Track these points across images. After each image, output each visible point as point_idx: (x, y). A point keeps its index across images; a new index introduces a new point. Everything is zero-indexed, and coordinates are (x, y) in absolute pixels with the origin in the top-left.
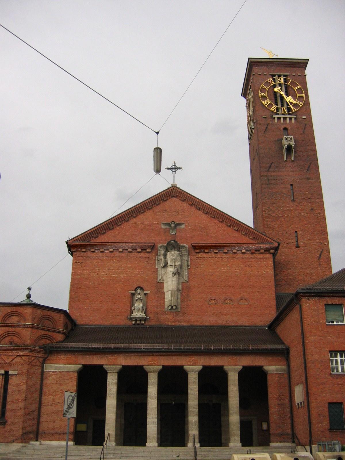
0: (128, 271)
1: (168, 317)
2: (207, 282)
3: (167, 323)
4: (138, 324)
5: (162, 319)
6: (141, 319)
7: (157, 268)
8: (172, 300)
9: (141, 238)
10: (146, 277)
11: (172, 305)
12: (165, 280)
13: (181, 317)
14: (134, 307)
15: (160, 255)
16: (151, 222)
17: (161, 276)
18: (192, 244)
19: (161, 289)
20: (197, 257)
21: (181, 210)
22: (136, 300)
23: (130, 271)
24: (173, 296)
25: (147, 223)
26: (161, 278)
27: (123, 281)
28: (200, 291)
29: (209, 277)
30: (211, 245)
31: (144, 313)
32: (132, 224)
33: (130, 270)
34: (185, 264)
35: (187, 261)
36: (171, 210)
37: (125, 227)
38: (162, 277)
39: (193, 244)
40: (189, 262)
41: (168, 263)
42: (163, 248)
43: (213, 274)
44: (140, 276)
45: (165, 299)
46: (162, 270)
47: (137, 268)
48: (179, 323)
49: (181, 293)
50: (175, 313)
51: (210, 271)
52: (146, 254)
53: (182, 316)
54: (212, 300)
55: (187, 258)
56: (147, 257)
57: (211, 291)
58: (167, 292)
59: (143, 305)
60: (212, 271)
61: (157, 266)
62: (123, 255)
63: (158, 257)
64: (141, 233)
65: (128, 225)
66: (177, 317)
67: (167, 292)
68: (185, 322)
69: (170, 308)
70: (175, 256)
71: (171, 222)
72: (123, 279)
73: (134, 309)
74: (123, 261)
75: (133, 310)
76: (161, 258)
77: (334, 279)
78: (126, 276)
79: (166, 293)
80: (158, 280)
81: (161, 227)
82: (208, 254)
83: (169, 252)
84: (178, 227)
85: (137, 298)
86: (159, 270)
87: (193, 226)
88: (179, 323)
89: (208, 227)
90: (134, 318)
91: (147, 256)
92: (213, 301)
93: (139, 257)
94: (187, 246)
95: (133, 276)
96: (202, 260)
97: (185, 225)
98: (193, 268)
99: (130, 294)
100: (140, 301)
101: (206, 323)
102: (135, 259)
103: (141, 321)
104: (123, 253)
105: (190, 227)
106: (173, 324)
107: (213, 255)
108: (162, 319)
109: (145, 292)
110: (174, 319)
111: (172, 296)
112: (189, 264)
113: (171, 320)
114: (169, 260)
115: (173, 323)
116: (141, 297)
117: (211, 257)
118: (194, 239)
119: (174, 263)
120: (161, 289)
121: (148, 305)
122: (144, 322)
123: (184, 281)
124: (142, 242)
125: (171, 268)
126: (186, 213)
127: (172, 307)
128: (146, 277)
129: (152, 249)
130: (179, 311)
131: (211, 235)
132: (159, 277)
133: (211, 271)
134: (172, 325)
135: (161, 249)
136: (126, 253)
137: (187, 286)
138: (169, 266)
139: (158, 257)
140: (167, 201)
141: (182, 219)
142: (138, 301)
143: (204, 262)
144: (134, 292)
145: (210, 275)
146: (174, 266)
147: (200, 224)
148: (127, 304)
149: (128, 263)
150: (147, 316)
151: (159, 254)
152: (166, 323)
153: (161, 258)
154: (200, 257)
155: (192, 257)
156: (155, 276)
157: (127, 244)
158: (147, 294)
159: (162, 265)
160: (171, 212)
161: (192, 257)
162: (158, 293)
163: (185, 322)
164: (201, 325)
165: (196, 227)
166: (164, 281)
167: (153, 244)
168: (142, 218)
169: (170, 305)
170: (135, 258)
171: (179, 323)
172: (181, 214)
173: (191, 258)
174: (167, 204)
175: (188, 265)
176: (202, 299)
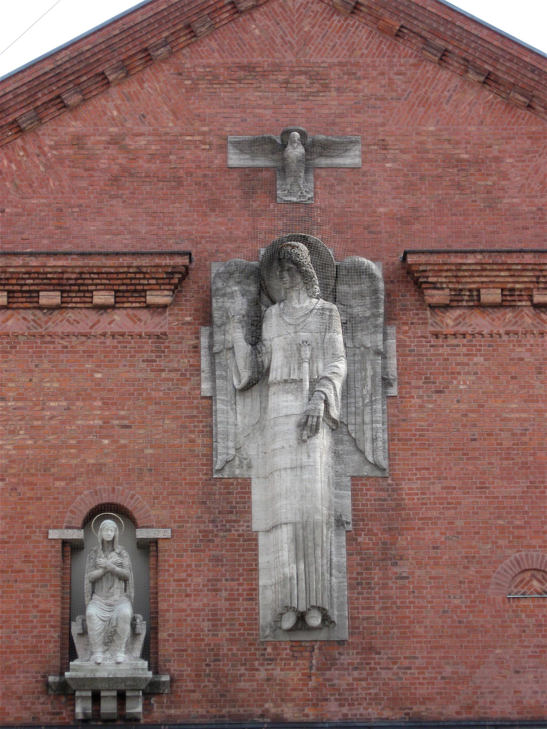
0: (42, 418)
1: (278, 673)
2: (497, 471)
3: (273, 710)
4: (109, 720)
5: (242, 685)
6: (122, 687)
7: (210, 398)
8: (302, 577)
9: (111, 223)
10: (149, 451)
11: (302, 607)
12: (254, 463)
13: (356, 674)
14: (79, 619)
15: (224, 324)
16: (166, 134)
17: (231, 444)
18: (404, 259)
19: (233, 517)
20: (438, 329)
21: (340, 64)
22: (95, 582)
23: (51, 418)
24: (305, 556)
25: (142, 142)
26: (232, 452)
27: (15, 475)
28: (459, 523)
29: (507, 444)
30: (513, 259)
31: (138, 653)
32: (56, 146)
33: (51, 408)
34: (370, 373)
35: (378, 353)
36: (277, 68)
37: (19, 164)
38: (237, 450)
39: (410, 259)
40: (393, 362)
41: (274, 365)
42: (239, 283)
43: (526, 425)
44: (114, 442)
45: (256, 570)
46: (239, 408)
47: (95, 399)
48: (341, 705)
49: (351, 539)
50: (320, 649)
51: (512, 411)
52: (144, 314)
53: (356, 669)
54: (529, 574)
55: (380, 337)
56: (149, 335)
57: (518, 523)
58: (268, 531)
59: (136, 609)
60: (524, 411)
61: (206, 387)
62: (10, 323)
63: (211, 335)
64: (112, 197)
65: (37, 151)
66: (328, 674)
67: (268, 531)
68: (376, 699)
69: (288, 622)
70: (313, 327)
71: (287, 133)
72: (13, 461)
73: (84, 633)
74: (11, 357)
75: (75, 640)
76: (229, 338)
77: (191, 474)
78: (30, 442)
79: (262, 540)
80: (218, 467)
81: (226, 159)
82: (498, 313)
83: (274, 303)
84: (324, 162)
85: (97, 572)
86: (219, 406)
87: (407, 157)
88: (345, 710)
89: (497, 160)
90: (83, 682)
91: (150, 330)
92: (535, 583)
93: (104, 335)
94: (376, 269)
95: (73, 442)
96: (464, 350)
97: (364, 153)
98: (414, 392)
99: (59, 546)
100: (118, 585)
101: (495, 708)
102: (81, 348)
103: (121, 697)
104: (9, 312)
105: (394, 161)
106: (311, 714)
107: (529, 321)
108: (242, 685)
109: (142, 534)
110: (312, 684)
111: (301, 554)
112: (393, 371)
113: (295, 694)
114: (275, 347)
115: (307, 711)
116: (121, 565)
117: (514, 328)
118: (417, 226)
119: (306, 365)
120: (233, 517)
121: (162, 606)
122: (144, 705)
123: (366, 471)
124: (118, 247)
125: (290, 397)
126: (365, 82)
127: (301, 618)
128: (149, 451)
129: (177, 289)
130: (341, 643)
131: (513, 205)
132: (220, 447)
133: (518, 411)
134: (305, 719)
135: (229, 290)
136: (29, 314)
137: (384, 495)
138: (279, 383)
139: (211, 335)
140: (256, 15)
141: (342, 115)
142: (105, 584)
143: (476, 359)
144: (76, 534)
145: (513, 435)
146: (307, 385)
147: (446, 146)
148: (42, 606)
149: (43, 371)
150: (156, 673)
151: (216, 314)
152: (267, 711)
153: (229, 338)
154: (452, 331)
155: (405, 332)
156: (199, 441)
157: (34, 262)
158: (153, 548)
159: (236, 382)
160: (281, 78)
161: (405, 332)
162: (217, 540)
163: (376, 699)
164: (471, 716)
165: (429, 160)
166: (249, 467)
167: (181, 261)
168: (115, 113)
169: (288, 608)
170: (82, 343)
171: (345, 710)
172: (338, 89)
173: (401, 336)
174: (257, 31)
175: (383, 379)
176: (472, 571)
